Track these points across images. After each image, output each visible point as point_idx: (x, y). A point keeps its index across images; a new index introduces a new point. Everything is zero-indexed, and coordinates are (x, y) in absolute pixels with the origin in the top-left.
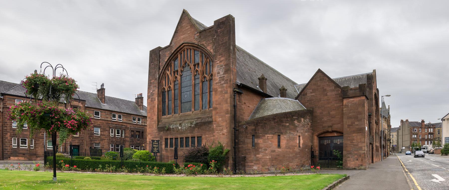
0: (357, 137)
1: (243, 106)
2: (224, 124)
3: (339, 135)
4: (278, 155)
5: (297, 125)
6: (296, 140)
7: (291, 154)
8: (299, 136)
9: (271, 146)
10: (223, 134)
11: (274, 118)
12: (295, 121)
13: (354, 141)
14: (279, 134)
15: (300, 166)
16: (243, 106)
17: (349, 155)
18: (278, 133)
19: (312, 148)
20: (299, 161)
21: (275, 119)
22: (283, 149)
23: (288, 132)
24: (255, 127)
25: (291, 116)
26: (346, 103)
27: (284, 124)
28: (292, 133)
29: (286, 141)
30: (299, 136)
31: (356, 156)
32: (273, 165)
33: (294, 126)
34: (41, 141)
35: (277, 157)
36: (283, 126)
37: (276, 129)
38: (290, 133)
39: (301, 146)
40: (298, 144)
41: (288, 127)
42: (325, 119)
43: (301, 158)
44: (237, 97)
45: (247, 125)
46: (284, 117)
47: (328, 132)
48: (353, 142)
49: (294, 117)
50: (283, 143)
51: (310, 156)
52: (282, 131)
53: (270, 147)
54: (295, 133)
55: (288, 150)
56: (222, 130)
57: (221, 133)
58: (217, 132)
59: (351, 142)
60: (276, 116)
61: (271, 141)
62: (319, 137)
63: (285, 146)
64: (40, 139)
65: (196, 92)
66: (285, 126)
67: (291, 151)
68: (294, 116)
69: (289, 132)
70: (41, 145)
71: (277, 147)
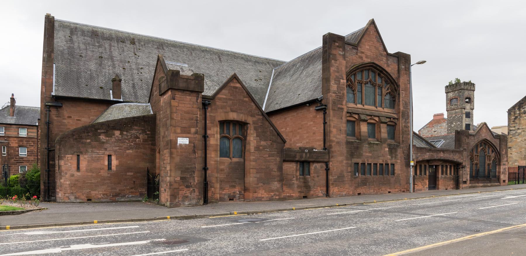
4: (78, 180)
5: (105, 141)
6: (102, 161)
7: (94, 179)
9: (70, 169)
11: (73, 134)
12: (100, 136)
14: (78, 154)
15: (110, 195)
18: (77, 152)
20: (109, 189)
21: (73, 135)
22: (83, 173)
23: (90, 150)
25: (93, 129)
27: (84, 140)
28: (95, 151)
29: (87, 163)
30: (110, 156)
32: (72, 193)
33: (97, 143)
34: (13, 167)
35: (76, 183)
37: (75, 147)
38: (92, 152)
39: (114, 168)
40: (106, 166)
41: (90, 145)
43: (113, 184)
44: (53, 112)
46: (84, 132)
49: (99, 131)
50: (83, 164)
52: (82, 149)
53: (70, 170)
54: (100, 151)
55: (90, 174)
60: (75, 131)
61: (70, 163)
63: (85, 168)
64: (12, 165)
65: (351, 47)
67: (94, 175)
68: (99, 129)
69: (91, 151)
70: (13, 171)
71: (76, 171)
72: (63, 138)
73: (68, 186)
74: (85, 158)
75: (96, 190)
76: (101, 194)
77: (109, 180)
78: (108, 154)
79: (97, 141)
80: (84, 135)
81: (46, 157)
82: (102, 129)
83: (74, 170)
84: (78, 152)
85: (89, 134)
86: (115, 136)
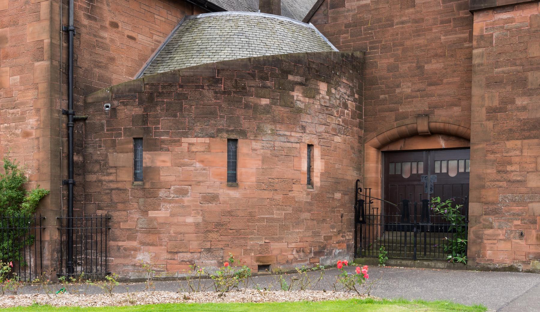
0: (522, 152)
1: (105, 34)
2: (30, 95)
3: (397, 147)
5: (302, 106)
6: (296, 159)
7: (278, 209)
8: (310, 146)
9: (201, 179)
10: (27, 135)
11: (214, 77)
12: (293, 91)
13: (509, 168)
14: (233, 137)
15: (311, 252)
16: (105, 34)
17: (491, 218)
18: (228, 131)
19: (357, 190)
22: (248, 191)
23: (268, 128)
24: (145, 110)
26: (482, 30)
27: (252, 99)
28: (281, 133)
30: (310, 146)
31: (518, 222)
32: (209, 250)
35: (226, 219)
36: (247, 106)
38: (274, 133)
39: (317, 180)
40: (303, 173)
41: (268, 112)
42: (406, 88)
43: (315, 222)
45: (116, 103)
47: (415, 134)
48: (506, 172)
49: (290, 77)
51: (350, 216)
52: (245, 125)
54: (293, 134)
55: (267, 194)
56: (22, 119)
57: (18, 132)
58: (6, 128)
59: (499, 172)
61: (202, 161)
62: (383, 152)
63: (254, 179)
66: (256, 108)
67: (279, 197)
68: (290, 72)
69: (272, 130)
72: (171, 85)
73: (192, 229)
74: (255, 150)
75: (282, 239)
76: (292, 251)
77: (309, 211)
78: (307, 142)
79: (285, 106)
80: (252, 83)
81: (65, 139)
82: (297, 74)
83: (218, 183)
84: (232, 131)
85: (268, 83)
86: (321, 96)
